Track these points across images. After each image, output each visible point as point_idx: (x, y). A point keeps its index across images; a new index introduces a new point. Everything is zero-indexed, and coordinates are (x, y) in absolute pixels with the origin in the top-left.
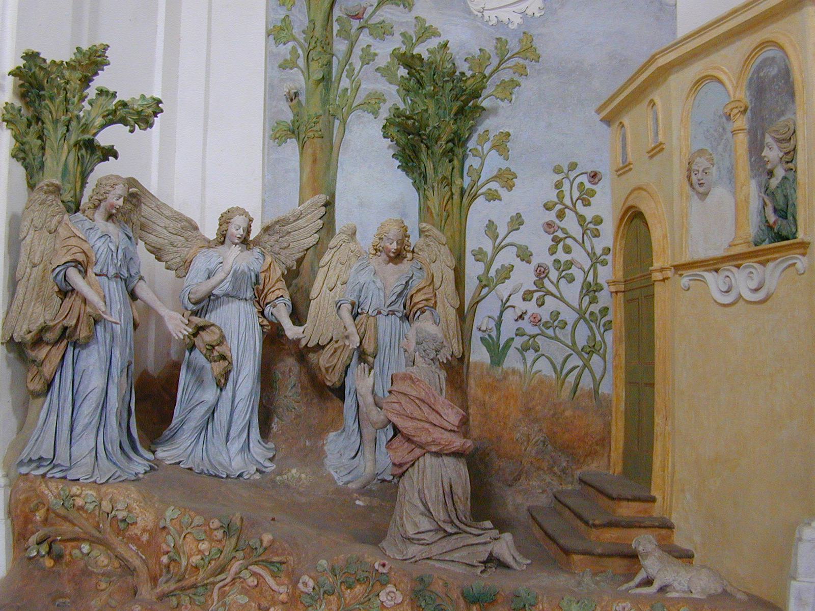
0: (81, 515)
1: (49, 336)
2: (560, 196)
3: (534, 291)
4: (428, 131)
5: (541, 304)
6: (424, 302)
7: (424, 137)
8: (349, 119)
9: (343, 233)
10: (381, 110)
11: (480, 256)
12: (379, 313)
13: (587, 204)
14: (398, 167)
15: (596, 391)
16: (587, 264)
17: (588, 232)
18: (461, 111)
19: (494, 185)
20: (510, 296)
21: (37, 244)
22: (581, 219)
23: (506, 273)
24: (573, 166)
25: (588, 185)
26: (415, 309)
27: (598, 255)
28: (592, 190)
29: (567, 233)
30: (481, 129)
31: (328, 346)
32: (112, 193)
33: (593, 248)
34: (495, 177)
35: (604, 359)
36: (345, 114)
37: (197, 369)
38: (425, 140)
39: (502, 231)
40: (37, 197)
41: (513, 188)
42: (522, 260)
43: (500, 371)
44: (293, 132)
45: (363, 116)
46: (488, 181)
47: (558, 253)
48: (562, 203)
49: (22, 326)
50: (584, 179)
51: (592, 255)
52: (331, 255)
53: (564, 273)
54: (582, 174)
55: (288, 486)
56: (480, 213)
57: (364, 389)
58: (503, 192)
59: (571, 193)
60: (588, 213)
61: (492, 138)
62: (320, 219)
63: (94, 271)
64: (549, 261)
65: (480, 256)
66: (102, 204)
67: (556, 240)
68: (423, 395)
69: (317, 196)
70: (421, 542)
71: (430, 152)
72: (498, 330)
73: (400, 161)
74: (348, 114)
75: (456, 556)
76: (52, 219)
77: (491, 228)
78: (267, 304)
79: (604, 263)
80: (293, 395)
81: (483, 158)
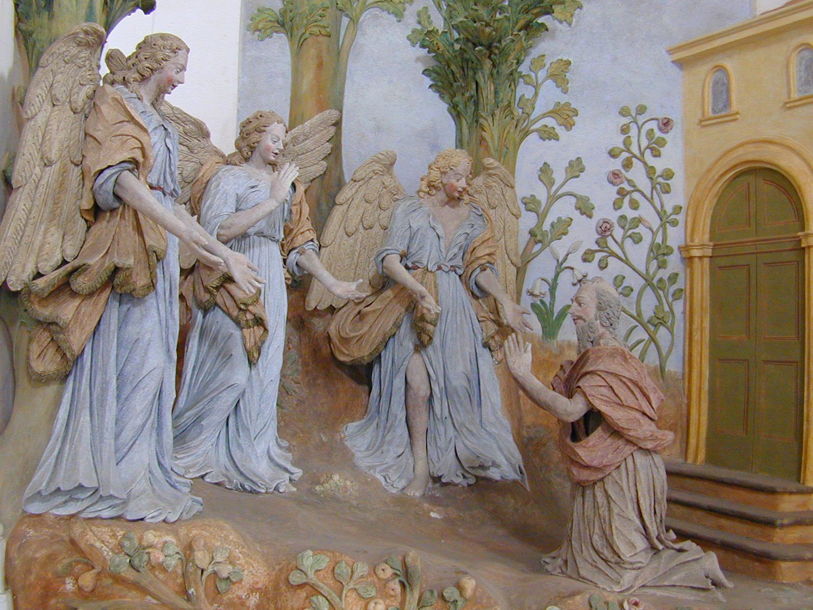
0: (156, 576)
1: (81, 283)
2: (627, 143)
3: (597, 251)
4: (504, 43)
5: (603, 266)
6: (486, 257)
7: (497, 51)
8: (362, 18)
9: (377, 162)
10: (406, 13)
11: (532, 206)
12: (439, 268)
13: (657, 154)
14: (430, 86)
15: (662, 369)
16: (655, 223)
17: (658, 187)
18: (527, 27)
19: (550, 122)
20: (567, 255)
21: (55, 127)
22: (650, 171)
23: (562, 228)
24: (641, 110)
25: (658, 134)
26: (475, 265)
27: (668, 214)
28: (663, 139)
29: (634, 186)
30: (534, 53)
31: (344, 309)
32: (172, 60)
33: (662, 206)
34: (550, 112)
35: (672, 333)
36: (358, 11)
37: (220, 337)
38: (496, 55)
39: (559, 176)
40: (64, 49)
41: (573, 127)
42: (582, 214)
43: (555, 344)
44: (283, 25)
45: (382, 17)
46: (544, 116)
47: (623, 208)
48: (629, 151)
49: (25, 265)
50: (653, 125)
51: (661, 214)
52: (354, 191)
53: (630, 232)
54: (652, 119)
55: (334, 499)
56: (532, 152)
57: (522, 368)
58: (560, 130)
59: (639, 141)
60: (659, 165)
61: (548, 66)
62: (328, 141)
63: (149, 181)
64: (613, 216)
65: (532, 206)
66: (153, 78)
67: (622, 193)
68: (635, 377)
69: (328, 111)
70: (635, 566)
71: (495, 71)
72: (553, 296)
73: (433, 80)
74: (362, 12)
75: (675, 578)
76: (80, 90)
77: (545, 171)
78: (293, 249)
79: (674, 223)
80: (292, 374)
81: (536, 87)
